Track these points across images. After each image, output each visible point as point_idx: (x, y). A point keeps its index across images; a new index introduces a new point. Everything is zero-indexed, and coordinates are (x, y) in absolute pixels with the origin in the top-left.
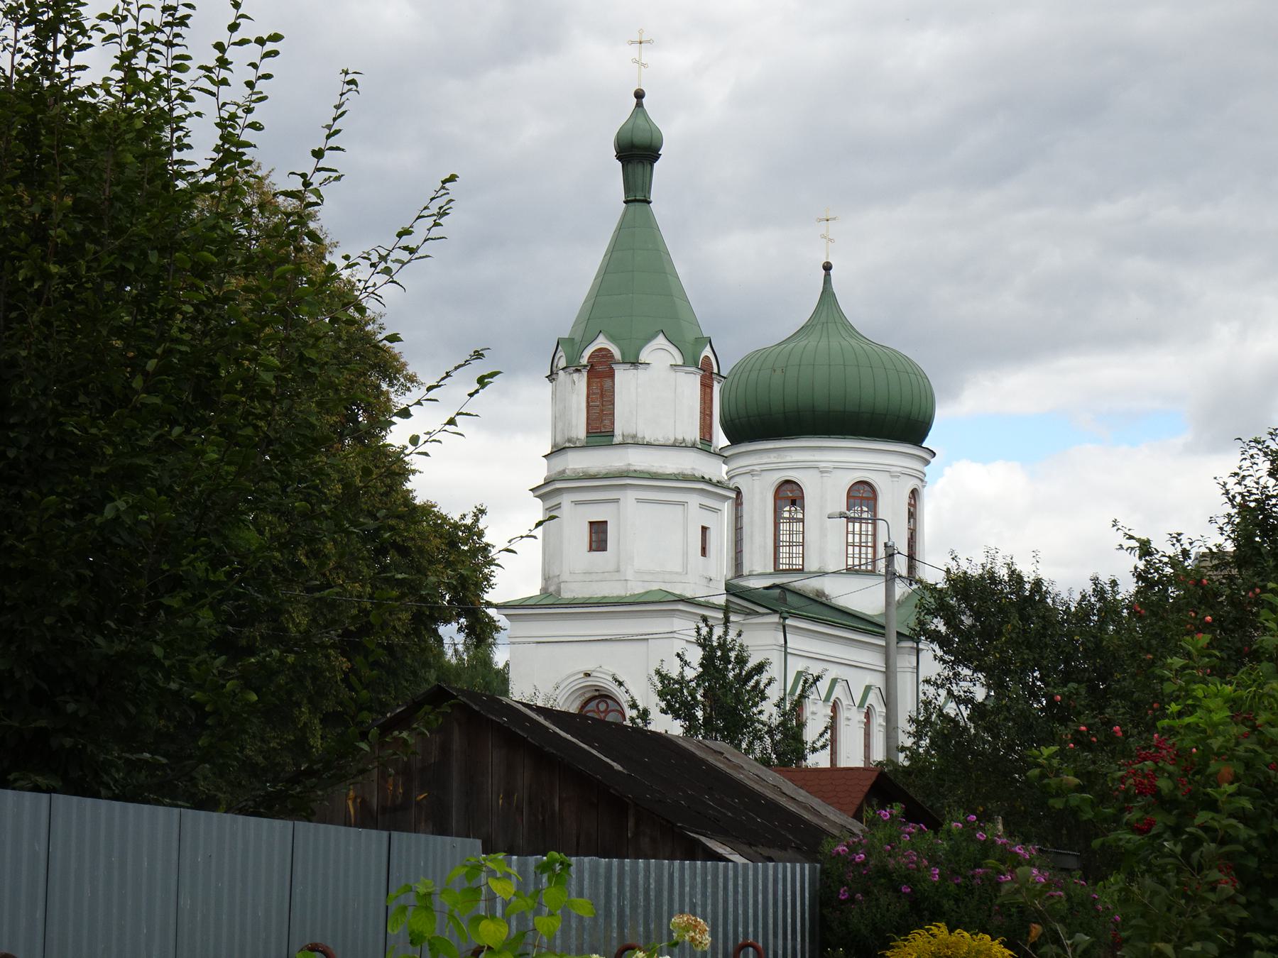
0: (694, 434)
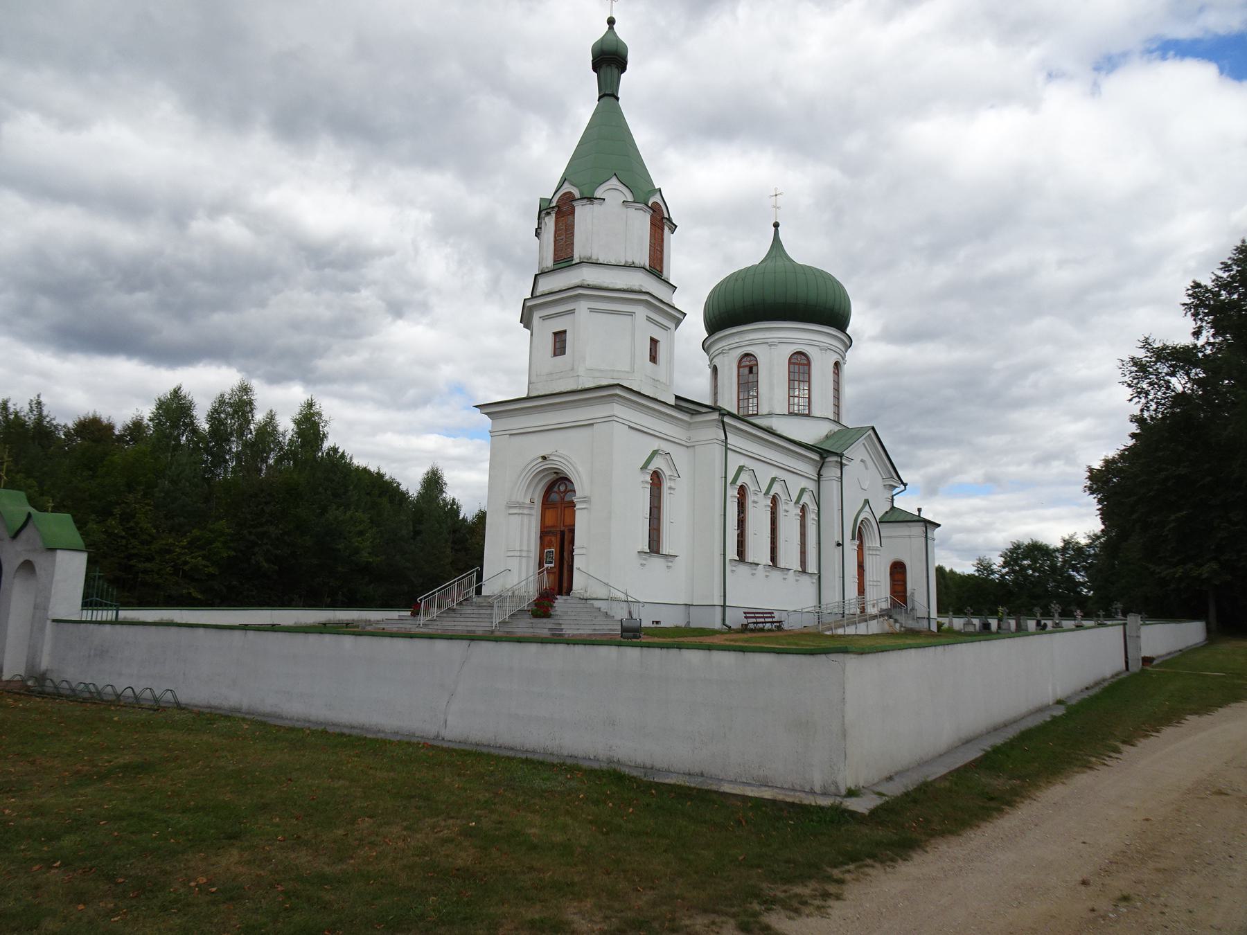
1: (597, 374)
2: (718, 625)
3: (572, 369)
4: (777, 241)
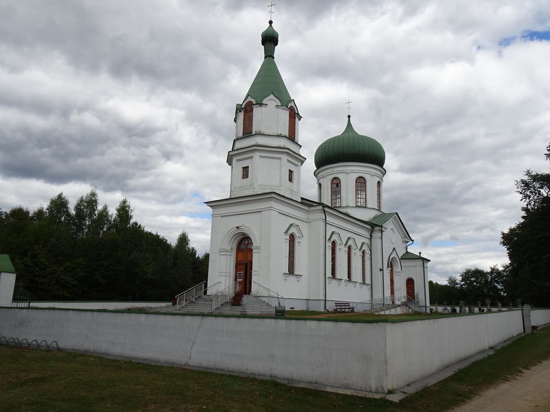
0: (287, 133)
1: (264, 187)
2: (322, 309)
3: (252, 185)
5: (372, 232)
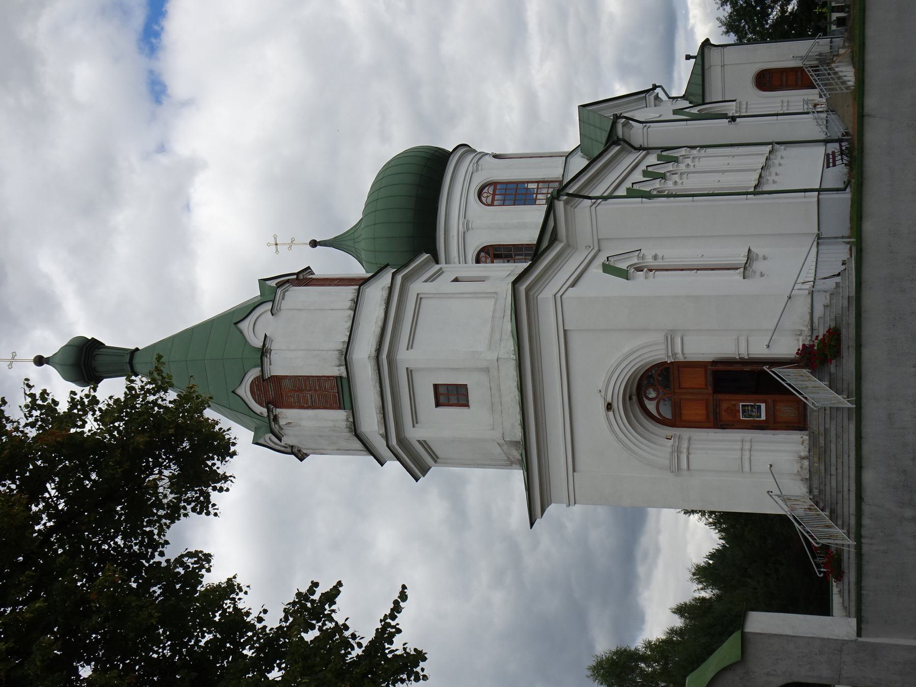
2: (847, 196)
3: (487, 370)
4: (334, 243)
5: (629, 146)
